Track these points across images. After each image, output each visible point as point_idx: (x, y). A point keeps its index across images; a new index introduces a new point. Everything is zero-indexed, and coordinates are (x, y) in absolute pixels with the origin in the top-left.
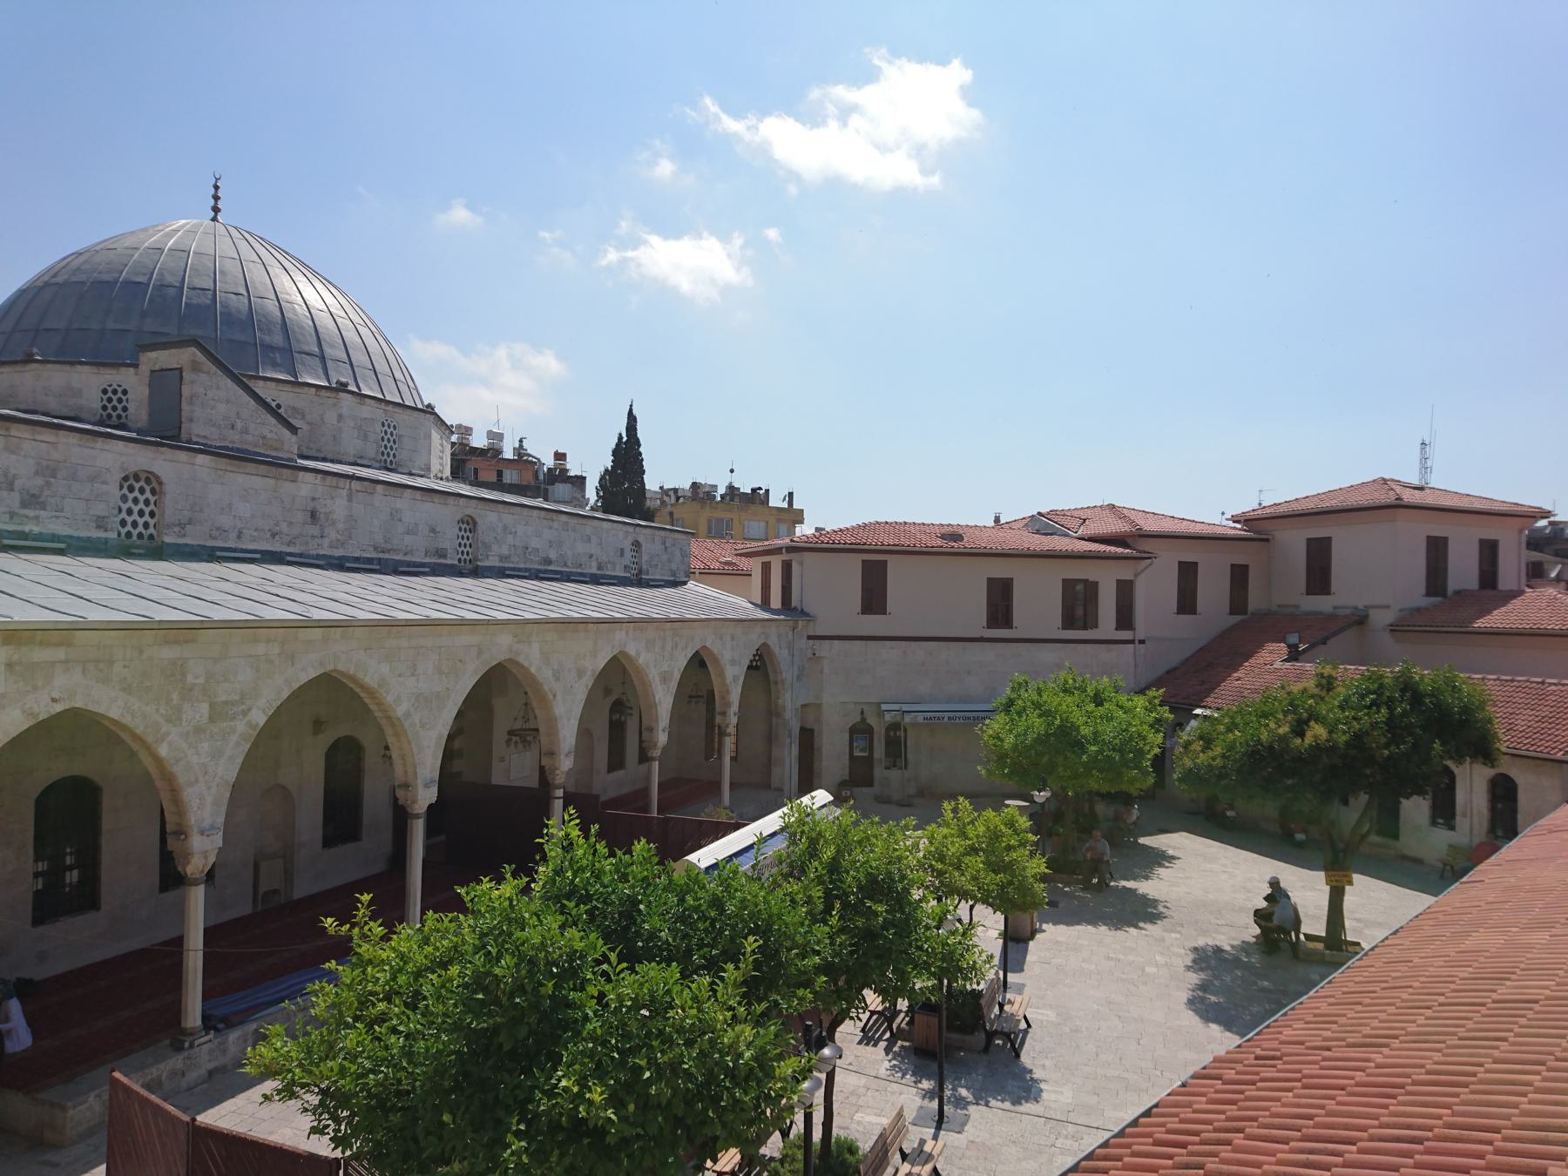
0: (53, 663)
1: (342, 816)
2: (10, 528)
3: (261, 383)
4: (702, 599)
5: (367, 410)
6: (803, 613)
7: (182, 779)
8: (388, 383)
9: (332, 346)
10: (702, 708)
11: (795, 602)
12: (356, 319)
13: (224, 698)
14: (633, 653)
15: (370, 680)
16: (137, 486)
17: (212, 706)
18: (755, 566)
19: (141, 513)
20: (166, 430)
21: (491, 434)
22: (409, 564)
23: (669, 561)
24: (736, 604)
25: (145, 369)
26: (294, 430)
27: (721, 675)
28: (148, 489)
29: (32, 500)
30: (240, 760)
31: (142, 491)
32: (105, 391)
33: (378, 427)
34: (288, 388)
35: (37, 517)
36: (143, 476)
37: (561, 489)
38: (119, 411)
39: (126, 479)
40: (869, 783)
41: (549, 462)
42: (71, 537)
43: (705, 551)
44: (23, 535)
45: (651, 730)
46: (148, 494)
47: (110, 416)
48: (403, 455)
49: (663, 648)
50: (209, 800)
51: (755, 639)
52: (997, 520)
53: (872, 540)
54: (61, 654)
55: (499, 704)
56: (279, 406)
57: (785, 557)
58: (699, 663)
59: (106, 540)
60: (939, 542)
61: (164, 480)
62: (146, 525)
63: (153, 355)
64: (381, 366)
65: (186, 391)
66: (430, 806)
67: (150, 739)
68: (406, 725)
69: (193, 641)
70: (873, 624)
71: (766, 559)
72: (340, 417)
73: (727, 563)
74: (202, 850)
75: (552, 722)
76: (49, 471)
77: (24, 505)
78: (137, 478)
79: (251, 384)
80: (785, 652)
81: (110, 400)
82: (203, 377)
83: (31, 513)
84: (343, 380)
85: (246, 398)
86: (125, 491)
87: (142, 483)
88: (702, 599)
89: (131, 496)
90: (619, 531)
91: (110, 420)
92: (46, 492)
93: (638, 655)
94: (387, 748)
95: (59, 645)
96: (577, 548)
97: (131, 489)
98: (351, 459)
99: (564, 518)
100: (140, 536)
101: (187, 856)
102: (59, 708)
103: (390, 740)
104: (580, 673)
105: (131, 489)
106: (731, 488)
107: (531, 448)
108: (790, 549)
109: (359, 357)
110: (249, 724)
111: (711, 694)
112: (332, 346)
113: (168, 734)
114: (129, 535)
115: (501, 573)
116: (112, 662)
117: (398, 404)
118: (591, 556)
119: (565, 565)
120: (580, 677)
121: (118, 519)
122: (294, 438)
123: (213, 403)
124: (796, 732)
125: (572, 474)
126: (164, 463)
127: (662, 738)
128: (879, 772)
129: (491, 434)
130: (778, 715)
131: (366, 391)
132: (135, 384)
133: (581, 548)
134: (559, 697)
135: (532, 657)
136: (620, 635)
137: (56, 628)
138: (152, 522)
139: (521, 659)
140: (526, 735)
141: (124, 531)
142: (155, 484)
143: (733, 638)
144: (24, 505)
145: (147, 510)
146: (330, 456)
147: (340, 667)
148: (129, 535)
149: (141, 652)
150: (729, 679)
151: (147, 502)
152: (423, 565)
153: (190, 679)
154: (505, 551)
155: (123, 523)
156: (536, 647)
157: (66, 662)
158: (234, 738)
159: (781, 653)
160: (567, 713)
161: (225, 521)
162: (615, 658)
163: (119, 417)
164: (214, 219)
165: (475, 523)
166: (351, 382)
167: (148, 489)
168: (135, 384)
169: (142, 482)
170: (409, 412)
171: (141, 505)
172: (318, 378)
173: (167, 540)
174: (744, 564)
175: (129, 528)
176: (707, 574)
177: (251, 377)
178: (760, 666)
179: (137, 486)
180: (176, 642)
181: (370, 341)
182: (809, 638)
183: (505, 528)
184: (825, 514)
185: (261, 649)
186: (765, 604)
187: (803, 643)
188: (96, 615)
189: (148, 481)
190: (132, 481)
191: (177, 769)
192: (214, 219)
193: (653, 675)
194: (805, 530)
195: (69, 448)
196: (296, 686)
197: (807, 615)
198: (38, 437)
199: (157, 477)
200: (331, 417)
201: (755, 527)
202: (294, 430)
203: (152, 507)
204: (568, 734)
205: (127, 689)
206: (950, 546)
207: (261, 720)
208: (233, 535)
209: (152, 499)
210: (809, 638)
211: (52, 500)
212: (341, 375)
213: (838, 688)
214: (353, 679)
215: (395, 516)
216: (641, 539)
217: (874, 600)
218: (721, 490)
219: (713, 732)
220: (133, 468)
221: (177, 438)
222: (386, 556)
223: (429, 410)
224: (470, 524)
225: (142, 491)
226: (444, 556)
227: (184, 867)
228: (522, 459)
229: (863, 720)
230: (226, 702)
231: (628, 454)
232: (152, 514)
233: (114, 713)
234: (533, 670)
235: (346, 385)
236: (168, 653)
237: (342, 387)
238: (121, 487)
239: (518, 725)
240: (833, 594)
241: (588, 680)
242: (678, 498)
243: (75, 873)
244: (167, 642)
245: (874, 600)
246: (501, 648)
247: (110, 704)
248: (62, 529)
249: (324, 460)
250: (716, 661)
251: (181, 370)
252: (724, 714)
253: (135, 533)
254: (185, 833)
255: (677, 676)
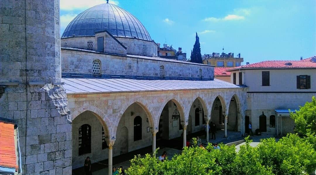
0: (83, 101)
1: (138, 134)
2: (73, 73)
3: (118, 38)
4: (218, 83)
5: (140, 42)
6: (246, 86)
7: (108, 125)
8: (144, 36)
9: (132, 29)
10: (218, 111)
11: (243, 83)
12: (137, 22)
13: (116, 108)
14: (201, 97)
15: (144, 104)
16: (96, 63)
17: (113, 110)
18: (232, 74)
19: (97, 68)
20: (101, 51)
21: (164, 45)
22: (150, 77)
23: (209, 73)
24: (230, 85)
25: (96, 37)
26: (126, 48)
27: (224, 102)
28: (98, 63)
29: (77, 67)
30: (119, 122)
31: (97, 64)
32: (88, 42)
33: (142, 46)
34: (124, 39)
35: (78, 70)
36: (97, 60)
37: (180, 57)
38: (91, 46)
39: (94, 61)
40: (265, 131)
41: (177, 50)
42: (84, 74)
43: (218, 71)
44: (76, 74)
45: (206, 116)
46: (98, 64)
47: (89, 48)
48: (148, 52)
49: (209, 96)
50: (113, 130)
51: (233, 93)
52: (301, 59)
53: (265, 66)
54: (84, 99)
55: (170, 109)
56: (122, 43)
57: (240, 71)
58: (218, 99)
59: (91, 74)
60: (285, 66)
61: (101, 61)
62: (98, 71)
63: (98, 34)
64: (143, 32)
65: (105, 42)
66: (157, 133)
67: (102, 117)
68: (152, 114)
69: (110, 96)
70: (266, 88)
71: (235, 72)
72: (135, 44)
73: (224, 73)
74: (112, 142)
75: (183, 114)
76: (80, 60)
77: (75, 68)
78: (96, 61)
79: (117, 38)
80: (241, 97)
81: (89, 44)
82: (108, 38)
83: (77, 69)
84: (135, 36)
85: (117, 42)
86: (94, 64)
87: (97, 62)
88: (218, 83)
89: (95, 65)
90: (196, 66)
91: (90, 48)
92: (79, 65)
93: (203, 97)
94: (147, 119)
95: (84, 97)
96: (187, 72)
97: (95, 63)
98: (137, 54)
99: (184, 64)
100: (97, 73)
101: (109, 142)
102: (85, 110)
103: (148, 117)
104: (189, 102)
105: (95, 63)
106: (223, 54)
107: (174, 48)
108: (241, 69)
109: (138, 31)
110: (120, 114)
111: (221, 107)
112: (132, 29)
113: (105, 116)
114: (95, 73)
115: (171, 78)
116: (94, 101)
117: (146, 41)
118: (190, 73)
119: (184, 76)
120: (189, 103)
121: (93, 70)
122: (126, 50)
123: (110, 43)
124: (244, 117)
125: (183, 53)
126: (102, 58)
127: (209, 118)
128: (268, 128)
129: (164, 45)
130: (239, 113)
131: (144, 39)
132: (94, 40)
133: (187, 71)
134: (184, 108)
135: (178, 99)
136: (198, 93)
137: (84, 94)
138: (99, 70)
139: (176, 99)
140: (177, 116)
141: (94, 72)
142: (99, 62)
143: (227, 93)
144: (75, 68)
145: (98, 68)
146: (132, 53)
147: (138, 101)
148: (95, 73)
149: (99, 99)
150: (226, 103)
151: (98, 66)
152: (153, 77)
153: (109, 104)
154: (170, 73)
155: (94, 71)
156: (179, 96)
157: (86, 101)
158: (117, 117)
159: (239, 98)
160: (186, 113)
161: (113, 69)
162: (197, 98)
163: (91, 48)
164: (107, 3)
165: (163, 67)
166: (137, 36)
167: (98, 63)
168: (94, 40)
169: (97, 62)
170: (149, 42)
171: (97, 67)
172: (130, 36)
173: (102, 74)
174: (229, 73)
175: (95, 72)
176: (218, 76)
177: (117, 37)
178: (234, 100)
179: (96, 63)
180: (106, 96)
181: (140, 27)
182: (248, 92)
183: (170, 67)
184: (251, 58)
185: (122, 97)
186: (235, 83)
187: (246, 94)
188: (91, 91)
189: (98, 61)
190: (95, 62)
191: (107, 123)
192: (107, 3)
193: (207, 103)
194: (244, 64)
195: (83, 55)
196: (129, 105)
197: (247, 86)
198: (77, 54)
199: (100, 60)
200: (133, 45)
201: (230, 62)
202: (126, 48)
203: (99, 67)
204: (186, 117)
205: (97, 107)
206: (289, 67)
207: (123, 113)
208: (115, 72)
209: (99, 65)
210: (248, 92)
211: (81, 67)
212: (134, 35)
213: (258, 105)
214: (140, 104)
215: (147, 66)
216: (202, 69)
217: (266, 81)
218: (221, 54)
219: (222, 118)
220: (95, 59)
221: (103, 52)
222: (145, 75)
223: (153, 41)
224: (162, 67)
225: (97, 64)
226: (157, 75)
227: (108, 144)
228: (171, 49)
229: (263, 114)
230: (116, 109)
231: (197, 47)
232: (99, 69)
233: (95, 112)
234: (178, 102)
235: (135, 37)
236: (105, 99)
237: (135, 38)
238: (93, 63)
239: (174, 114)
240: (255, 80)
241: (191, 104)
242: (209, 57)
243: (305, 80)
244: (104, 96)
245: (266, 81)
246: (171, 97)
247: (94, 109)
248: (82, 72)
249: (131, 54)
250: (222, 99)
251: (103, 37)
252: (224, 112)
253: (96, 73)
254: (108, 137)
255: (212, 103)
